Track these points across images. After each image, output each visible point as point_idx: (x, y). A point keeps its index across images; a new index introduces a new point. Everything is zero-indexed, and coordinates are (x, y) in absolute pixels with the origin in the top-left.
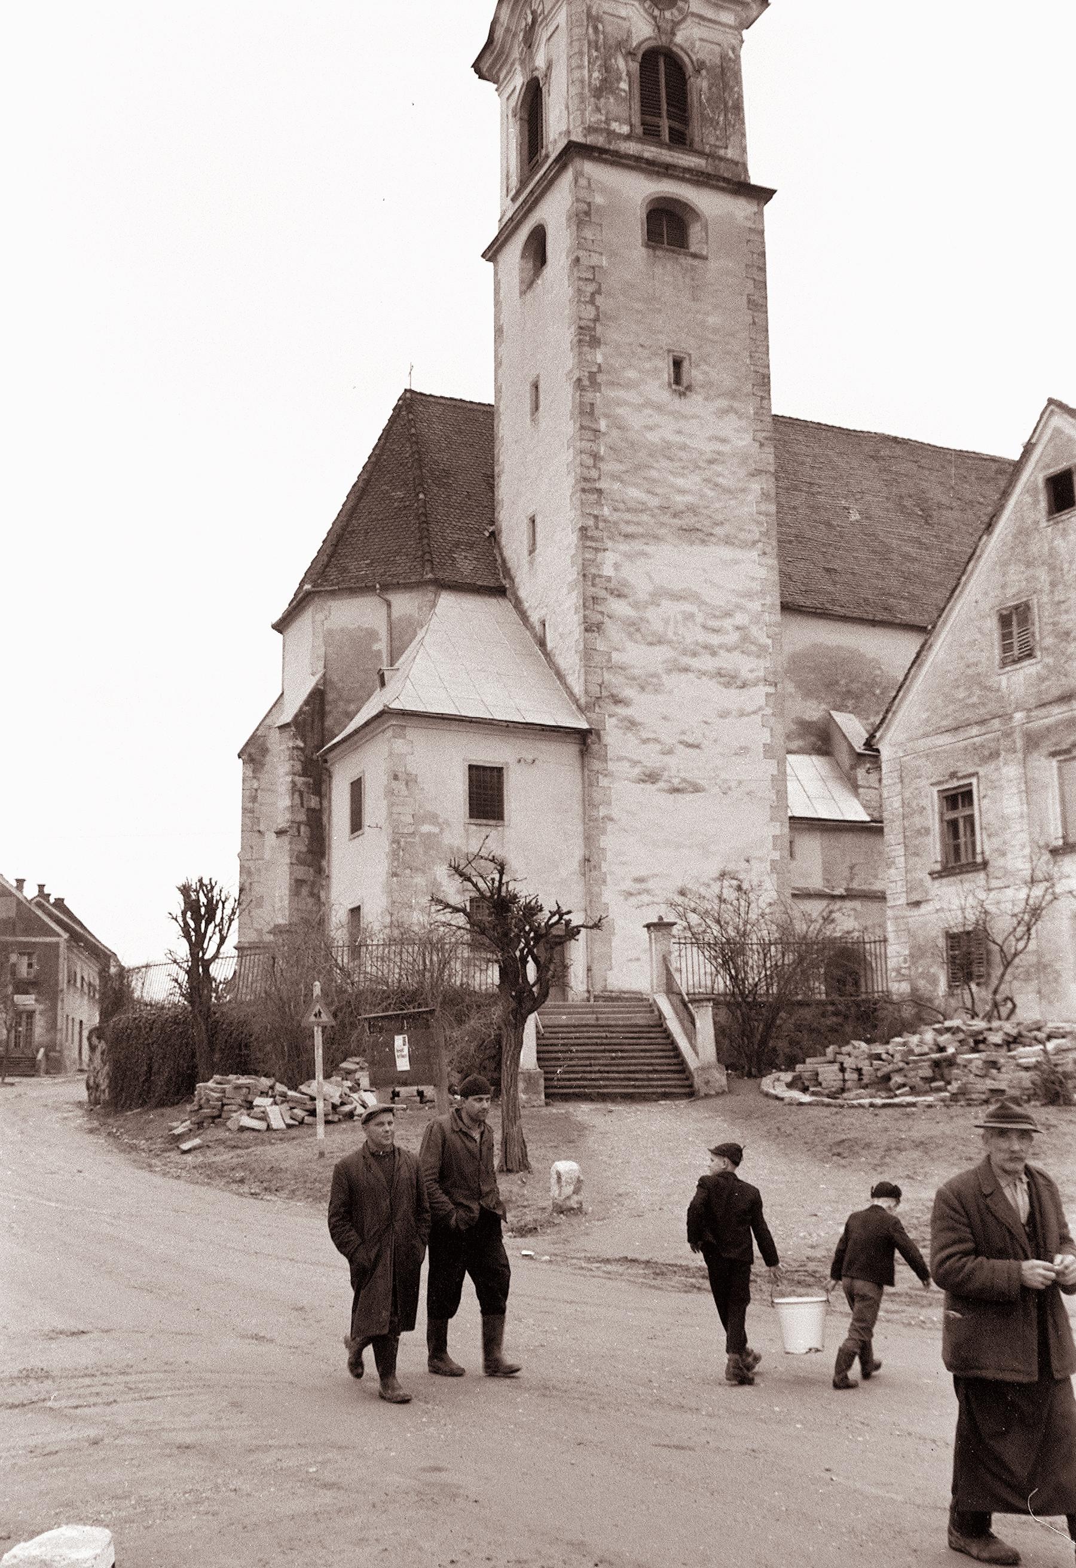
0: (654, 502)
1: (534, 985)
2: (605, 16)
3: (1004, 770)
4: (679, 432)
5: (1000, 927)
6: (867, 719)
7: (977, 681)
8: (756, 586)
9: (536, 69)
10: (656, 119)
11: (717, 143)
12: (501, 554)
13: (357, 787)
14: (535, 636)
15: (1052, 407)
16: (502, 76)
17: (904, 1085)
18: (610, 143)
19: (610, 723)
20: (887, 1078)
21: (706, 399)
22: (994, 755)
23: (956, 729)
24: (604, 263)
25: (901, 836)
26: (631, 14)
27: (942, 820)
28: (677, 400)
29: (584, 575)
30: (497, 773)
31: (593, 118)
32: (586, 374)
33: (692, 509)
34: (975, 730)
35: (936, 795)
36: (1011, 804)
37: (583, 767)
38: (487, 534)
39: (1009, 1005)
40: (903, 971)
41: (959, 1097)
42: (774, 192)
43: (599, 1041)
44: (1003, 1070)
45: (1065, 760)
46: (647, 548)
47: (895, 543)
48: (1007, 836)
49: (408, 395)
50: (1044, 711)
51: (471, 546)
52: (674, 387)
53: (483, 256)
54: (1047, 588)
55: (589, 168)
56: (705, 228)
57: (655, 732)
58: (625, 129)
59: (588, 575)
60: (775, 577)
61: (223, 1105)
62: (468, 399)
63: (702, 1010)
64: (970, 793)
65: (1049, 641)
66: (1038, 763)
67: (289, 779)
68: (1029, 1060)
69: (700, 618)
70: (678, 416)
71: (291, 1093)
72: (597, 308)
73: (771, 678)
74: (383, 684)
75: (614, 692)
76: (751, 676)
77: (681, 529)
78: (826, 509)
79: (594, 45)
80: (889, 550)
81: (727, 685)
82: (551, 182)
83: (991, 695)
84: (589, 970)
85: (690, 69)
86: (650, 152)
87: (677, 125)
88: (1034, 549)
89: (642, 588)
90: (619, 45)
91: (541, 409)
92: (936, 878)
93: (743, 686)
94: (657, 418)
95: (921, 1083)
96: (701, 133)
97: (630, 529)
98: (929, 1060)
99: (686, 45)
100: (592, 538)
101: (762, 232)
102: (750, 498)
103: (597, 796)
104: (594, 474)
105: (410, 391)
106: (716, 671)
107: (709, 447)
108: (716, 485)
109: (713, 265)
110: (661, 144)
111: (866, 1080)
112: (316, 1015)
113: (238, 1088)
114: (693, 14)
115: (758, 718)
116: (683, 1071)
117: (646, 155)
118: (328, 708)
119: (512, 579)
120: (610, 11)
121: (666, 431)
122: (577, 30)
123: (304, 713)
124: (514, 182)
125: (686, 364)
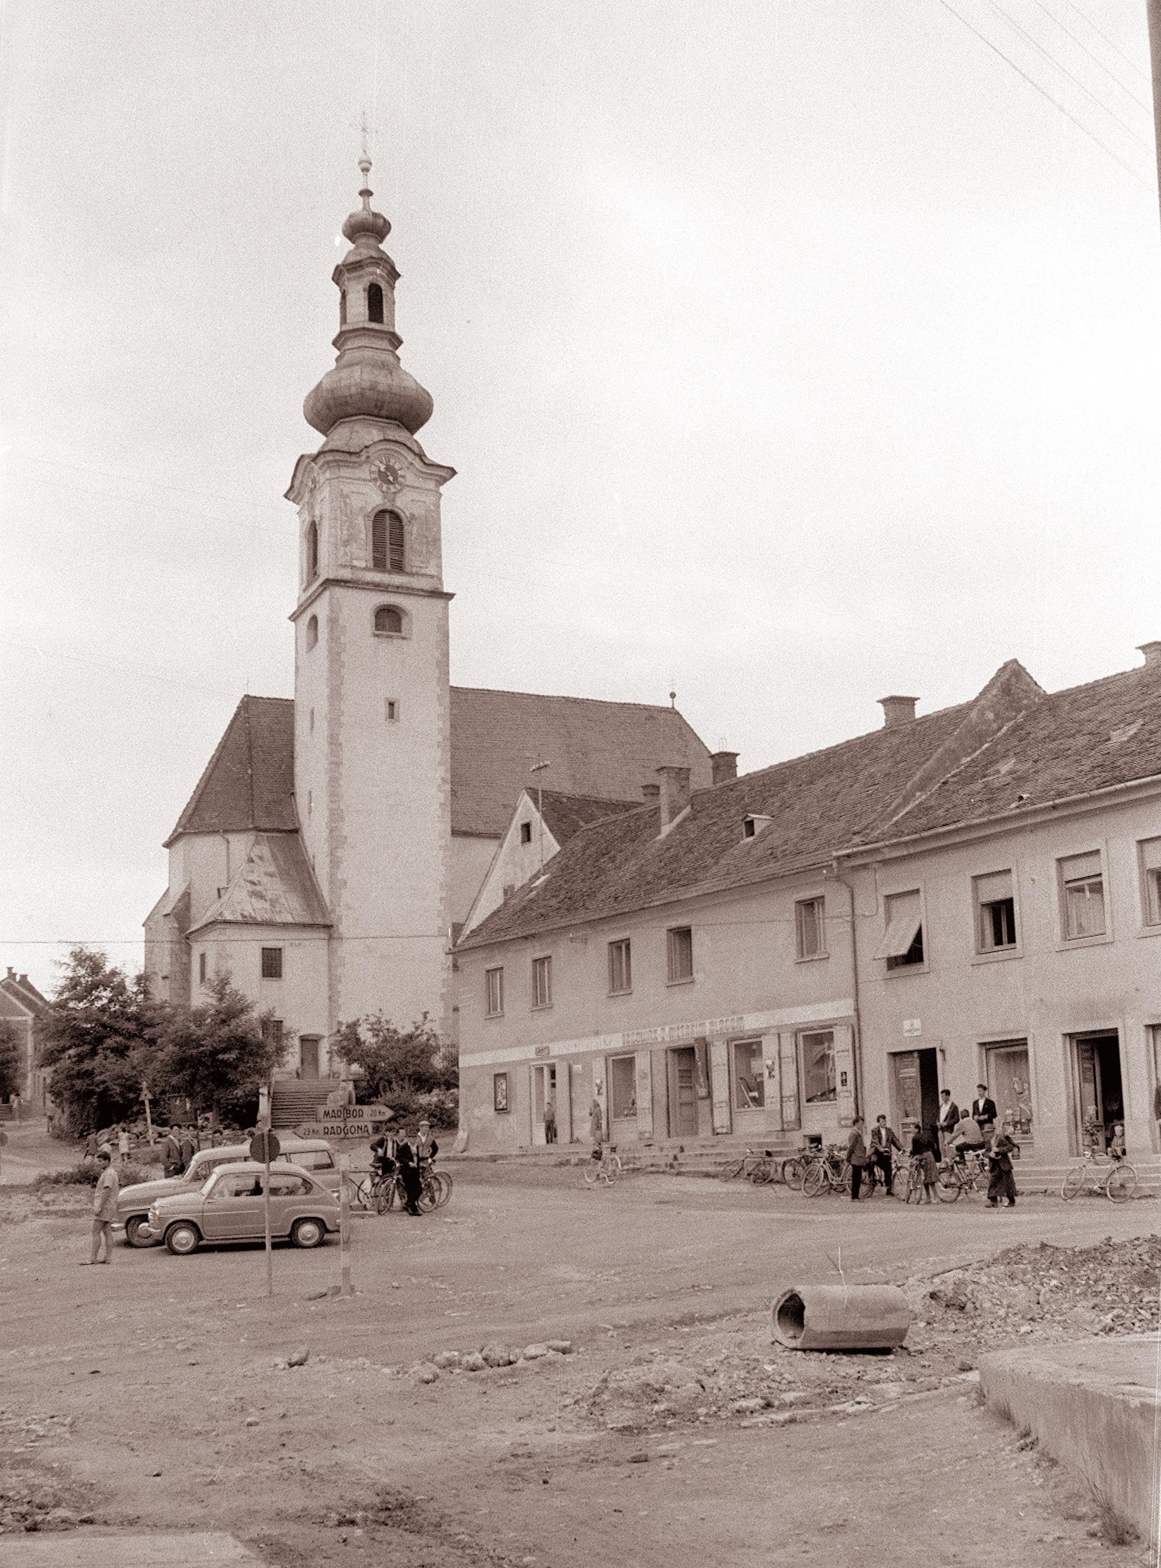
13: (203, 956)
42: (454, 595)
58: (363, 565)
96: (412, 560)
114: (407, 486)
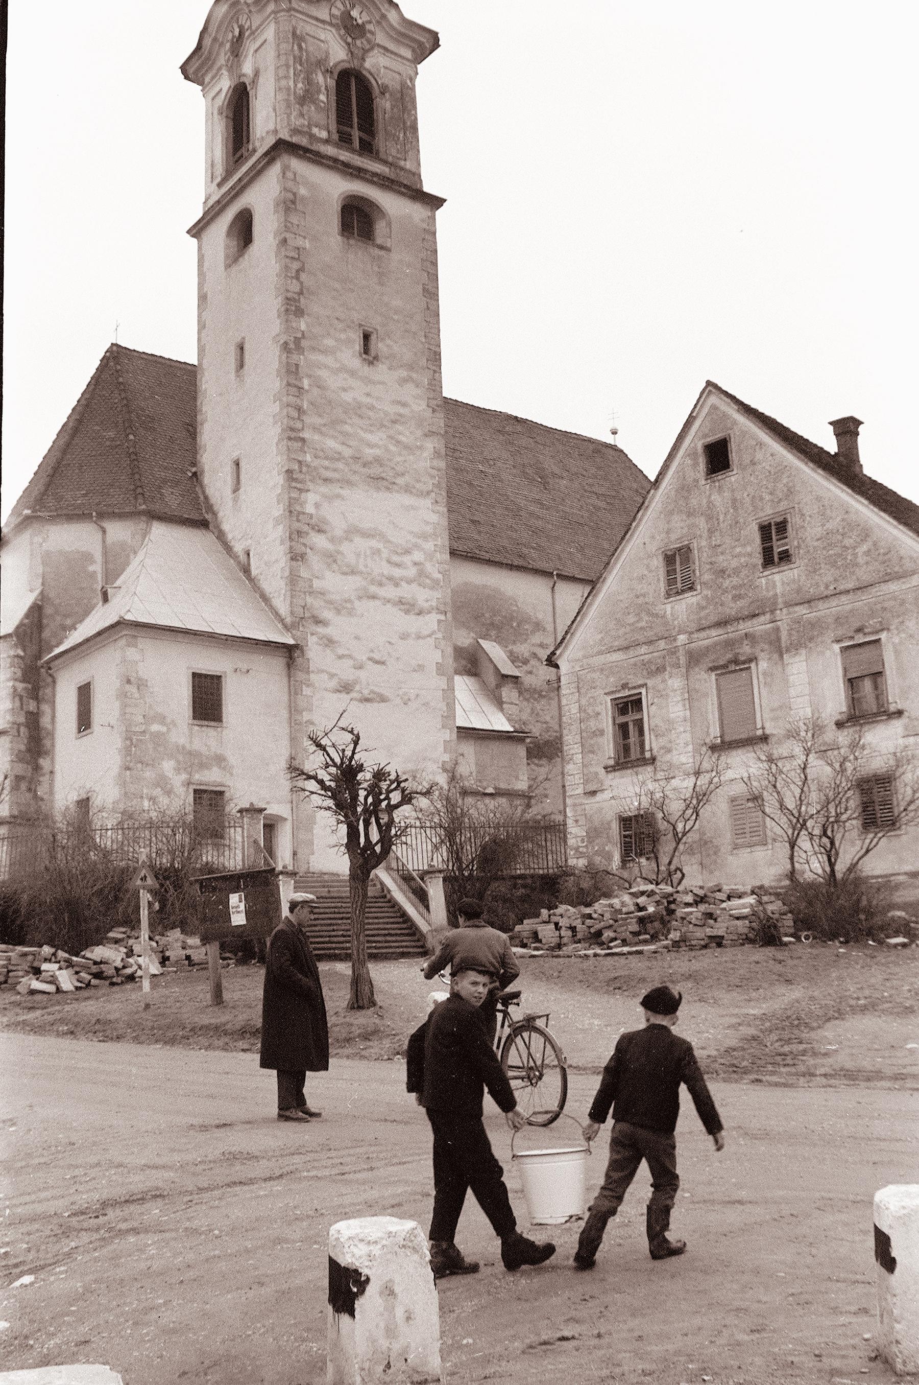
0: (347, 452)
1: (377, 844)
2: (307, 37)
3: (670, 682)
4: (368, 395)
5: (675, 807)
6: (506, 647)
7: (645, 609)
8: (429, 529)
9: (244, 75)
10: (349, 129)
11: (399, 156)
12: (204, 492)
13: (85, 693)
14: (239, 563)
15: (710, 388)
16: (207, 79)
17: (615, 939)
18: (311, 144)
19: (312, 641)
20: (599, 933)
21: (390, 369)
22: (660, 670)
23: (627, 648)
24: (308, 246)
25: (578, 737)
26: (329, 38)
27: (614, 724)
28: (366, 368)
29: (291, 512)
30: (216, 680)
31: (300, 122)
32: (293, 339)
33: (378, 461)
34: (643, 649)
35: (609, 704)
36: (676, 710)
37: (289, 677)
38: (190, 474)
39: (679, 875)
40: (581, 849)
41: (682, 944)
42: (445, 200)
43: (336, 910)
44: (719, 920)
45: (722, 674)
46: (342, 492)
47: (523, 503)
48: (673, 736)
49: (115, 348)
50: (703, 634)
51: (177, 483)
52: (364, 356)
53: (188, 232)
54: (705, 535)
55: (297, 164)
56: (389, 224)
57: (348, 649)
58: (324, 135)
59: (293, 511)
60: (444, 522)
61: (9, 972)
62: (167, 357)
63: (435, 881)
64: (639, 701)
65: (707, 577)
66: (698, 676)
67: (11, 684)
68: (744, 911)
69: (385, 553)
70: (368, 381)
71: (75, 959)
72: (302, 283)
73: (442, 608)
74: (106, 599)
75: (315, 612)
76: (426, 605)
77: (369, 477)
78: (467, 472)
79: (298, 60)
80: (520, 509)
81: (407, 612)
82: (260, 172)
83: (658, 621)
84: (295, 854)
85: (376, 91)
86: (344, 156)
87: (365, 136)
88: (694, 502)
89: (338, 526)
90: (319, 63)
91: (246, 367)
92: (611, 771)
93: (420, 613)
94: (351, 382)
95: (631, 936)
97: (329, 474)
98: (636, 917)
99: (372, 71)
100: (296, 480)
101: (435, 233)
102: (425, 454)
103: (302, 702)
104: (299, 425)
105: (116, 345)
106: (397, 599)
107: (393, 410)
108: (399, 442)
109: (395, 256)
110: (353, 151)
111: (580, 936)
112: (142, 879)
113: (25, 955)
114: (379, 45)
115: (431, 641)
116: (414, 934)
117: (342, 158)
118: (45, 621)
119: (215, 514)
120: (311, 33)
121: (356, 393)
122: (284, 46)
123: (25, 625)
124: (220, 171)
125: (373, 338)
